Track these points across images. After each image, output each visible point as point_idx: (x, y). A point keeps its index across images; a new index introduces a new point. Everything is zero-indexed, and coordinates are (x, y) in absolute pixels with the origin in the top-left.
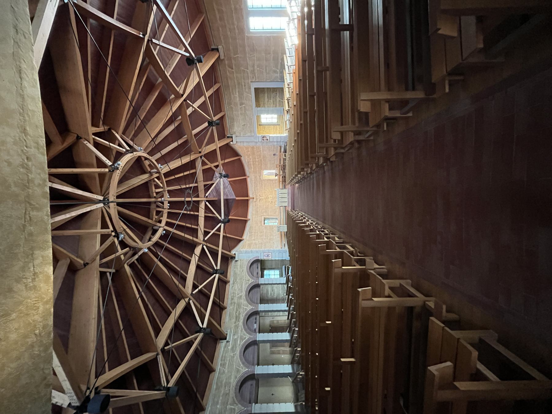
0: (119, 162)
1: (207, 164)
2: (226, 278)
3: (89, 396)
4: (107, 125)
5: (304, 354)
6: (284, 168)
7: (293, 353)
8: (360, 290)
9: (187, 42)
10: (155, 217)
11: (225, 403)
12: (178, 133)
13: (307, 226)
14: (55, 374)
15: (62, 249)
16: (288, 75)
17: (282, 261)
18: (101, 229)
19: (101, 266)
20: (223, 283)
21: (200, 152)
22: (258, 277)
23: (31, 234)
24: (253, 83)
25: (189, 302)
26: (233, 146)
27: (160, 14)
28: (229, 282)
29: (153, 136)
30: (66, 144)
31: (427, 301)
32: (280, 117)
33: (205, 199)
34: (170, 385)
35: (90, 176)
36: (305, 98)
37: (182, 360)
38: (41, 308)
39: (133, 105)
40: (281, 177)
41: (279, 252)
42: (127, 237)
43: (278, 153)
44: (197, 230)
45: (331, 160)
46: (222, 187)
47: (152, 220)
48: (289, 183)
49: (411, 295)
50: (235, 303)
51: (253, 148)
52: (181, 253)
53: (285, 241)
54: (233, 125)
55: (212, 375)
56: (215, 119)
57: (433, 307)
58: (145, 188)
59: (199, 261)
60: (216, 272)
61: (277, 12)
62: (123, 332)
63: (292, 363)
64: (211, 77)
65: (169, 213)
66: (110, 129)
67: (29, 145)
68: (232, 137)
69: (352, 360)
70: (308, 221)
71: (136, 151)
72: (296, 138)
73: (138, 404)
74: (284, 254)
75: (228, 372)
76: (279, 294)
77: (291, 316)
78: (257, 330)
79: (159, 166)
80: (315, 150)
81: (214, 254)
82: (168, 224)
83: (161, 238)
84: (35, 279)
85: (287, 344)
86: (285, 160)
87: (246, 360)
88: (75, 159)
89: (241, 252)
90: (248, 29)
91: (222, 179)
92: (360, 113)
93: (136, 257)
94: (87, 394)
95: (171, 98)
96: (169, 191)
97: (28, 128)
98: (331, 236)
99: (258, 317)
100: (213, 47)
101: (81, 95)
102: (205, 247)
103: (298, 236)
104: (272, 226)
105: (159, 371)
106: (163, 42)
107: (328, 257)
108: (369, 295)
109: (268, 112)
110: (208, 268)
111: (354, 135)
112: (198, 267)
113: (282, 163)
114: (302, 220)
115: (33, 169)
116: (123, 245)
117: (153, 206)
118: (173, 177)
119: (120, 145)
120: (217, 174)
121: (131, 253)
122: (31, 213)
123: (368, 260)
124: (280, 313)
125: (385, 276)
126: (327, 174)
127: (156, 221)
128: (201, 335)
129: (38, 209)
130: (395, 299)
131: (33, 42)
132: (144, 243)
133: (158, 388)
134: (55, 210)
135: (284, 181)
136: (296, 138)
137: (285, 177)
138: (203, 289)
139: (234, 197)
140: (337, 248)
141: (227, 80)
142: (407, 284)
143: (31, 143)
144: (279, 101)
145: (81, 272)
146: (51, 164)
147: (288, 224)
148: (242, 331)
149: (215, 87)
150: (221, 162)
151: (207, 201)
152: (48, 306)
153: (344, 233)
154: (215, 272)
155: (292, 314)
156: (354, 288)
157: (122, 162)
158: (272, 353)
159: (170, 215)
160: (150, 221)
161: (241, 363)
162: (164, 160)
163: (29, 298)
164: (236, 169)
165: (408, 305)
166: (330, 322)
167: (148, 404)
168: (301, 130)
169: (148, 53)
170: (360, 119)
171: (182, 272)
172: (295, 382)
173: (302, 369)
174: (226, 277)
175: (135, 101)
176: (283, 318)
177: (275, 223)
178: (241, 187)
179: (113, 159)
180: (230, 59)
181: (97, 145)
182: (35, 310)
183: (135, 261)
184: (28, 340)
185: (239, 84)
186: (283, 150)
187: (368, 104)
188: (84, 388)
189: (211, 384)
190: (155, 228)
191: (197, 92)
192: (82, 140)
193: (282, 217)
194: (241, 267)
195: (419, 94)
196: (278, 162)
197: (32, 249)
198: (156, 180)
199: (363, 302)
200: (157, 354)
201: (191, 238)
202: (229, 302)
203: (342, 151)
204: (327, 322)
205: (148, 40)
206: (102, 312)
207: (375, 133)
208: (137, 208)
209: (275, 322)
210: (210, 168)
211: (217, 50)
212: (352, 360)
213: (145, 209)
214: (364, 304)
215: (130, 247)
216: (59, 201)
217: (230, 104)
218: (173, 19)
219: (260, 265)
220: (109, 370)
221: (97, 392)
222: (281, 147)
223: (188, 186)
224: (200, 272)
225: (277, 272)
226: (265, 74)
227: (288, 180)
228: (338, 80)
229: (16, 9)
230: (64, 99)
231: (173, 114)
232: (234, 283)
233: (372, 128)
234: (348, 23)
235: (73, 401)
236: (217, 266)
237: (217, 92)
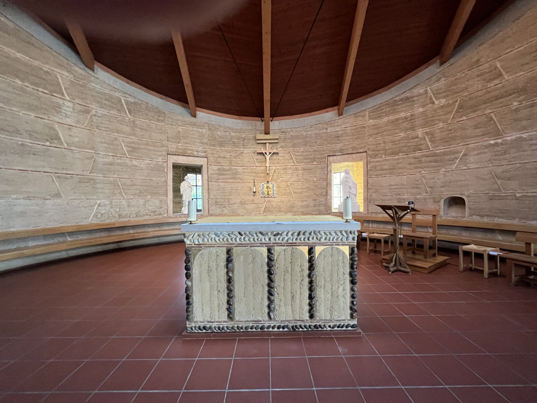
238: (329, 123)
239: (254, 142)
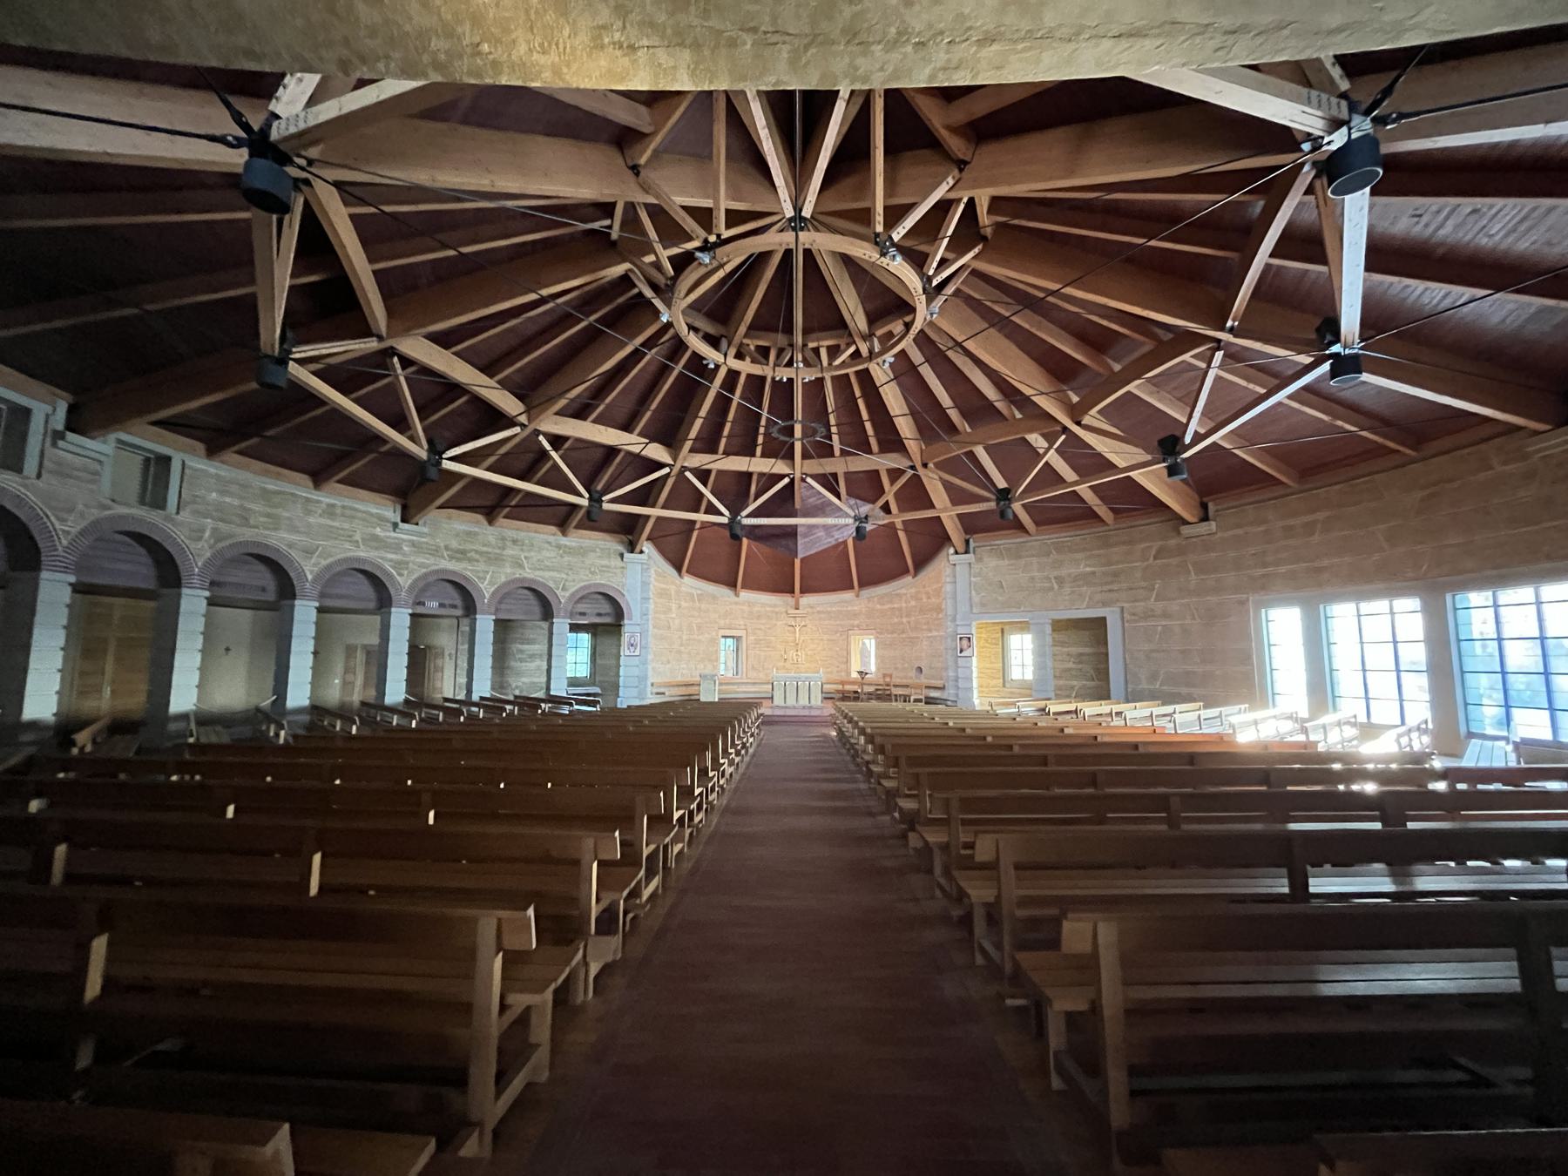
0: (899, 258)
1: (892, 482)
2: (577, 527)
3: (291, 163)
4: (995, 232)
5: (340, 744)
6: (883, 696)
7: (344, 713)
8: (531, 912)
9: (1223, 438)
10: (752, 344)
11: (221, 513)
12: (978, 410)
13: (715, 760)
14: (361, 84)
15: (682, 109)
16: (1146, 713)
17: (616, 687)
18: (728, 211)
19: (631, 207)
20: (562, 517)
22: (571, 615)
23: (733, 43)
24: (1118, 616)
26: (943, 554)
27: (1290, 372)
28: (564, 534)
29: (969, 345)
30: (944, 135)
31: (481, 1134)
32: (1026, 689)
33: (798, 475)
34: (293, 368)
35: (866, 187)
36: (1083, 760)
37: (356, 401)
38: (542, 59)
39: (1050, 299)
40: (855, 688)
41: (643, 678)
42: (702, 271)
43: (924, 681)
44: (714, 451)
45: (911, 835)
46: (830, 521)
47: (746, 336)
48: (839, 709)
49: (502, 1079)
51: (939, 609)
52: (654, 406)
53: (671, 695)
54: (1001, 556)
55: (305, 479)
57: (463, 1153)
58: (829, 320)
59: (629, 453)
60: (596, 499)
61: (1321, 688)
62: (452, 253)
63: (316, 710)
64: (1131, 500)
66: (984, 239)
67: (955, 48)
68: (967, 552)
69: (314, 889)
70: (731, 763)
71: (929, 301)
72: (968, 731)
73: (252, 281)
74: (634, 692)
75: (309, 525)
76: (519, 674)
77: (452, 709)
78: (420, 610)
79: (889, 358)
80: (932, 785)
81: (644, 496)
82: (733, 375)
83: (697, 358)
84: (621, 47)
85: (371, 694)
86: (906, 699)
87: (339, 574)
88: (909, 153)
89: (645, 570)
90: (1269, 604)
91: (851, 521)
92: (1057, 922)
93: (648, 293)
94: (297, 160)
95: (1070, 393)
96: (820, 381)
97: (995, 47)
98: (688, 831)
99: (459, 612)
100: (1211, 507)
101: (1070, 173)
102: (667, 470)
103: (686, 734)
104: (717, 660)
105: (343, 339)
106: (1218, 379)
107: (626, 820)
108: (512, 942)
109: (1039, 653)
110: (606, 478)
111: (987, 905)
112: (612, 451)
113: (899, 691)
114: (734, 745)
115: (895, 56)
116: (683, 262)
117: (781, 339)
118: (858, 393)
119: (943, 262)
120: (865, 509)
121: (661, 281)
122: (786, 48)
123: (615, 941)
124: (468, 677)
125: (562, 997)
126: (868, 821)
127: (741, 344)
128: (422, 453)
129: (793, 62)
130: (493, 1025)
131: (1208, 66)
132: (683, 312)
133: (289, 334)
134: (779, 103)
135: (845, 697)
136: (968, 731)
137: (856, 699)
139: (800, 555)
140: (652, 847)
141: (1124, 543)
142: (537, 1067)
143: (960, 51)
144: (1073, 688)
146: (893, 96)
147: (723, 703)
148: (422, 565)
149: (1102, 511)
151: (792, 480)
152: (547, 75)
153: (693, 872)
154: (596, 496)
155: (459, 712)
156: (536, 897)
157: (899, 266)
158: (350, 651)
159: (756, 382)
160: (743, 329)
161: (330, 560)
162: (904, 370)
163: (574, 33)
164: (877, 562)
165: (473, 1070)
166: (431, 822)
167: (247, 311)
168: (991, 746)
169: (1194, 340)
170: (1034, 923)
171: (601, 408)
172: (256, 716)
173: (295, 737)
174: (578, 527)
175: (1060, 303)
176: (447, 685)
177: (724, 669)
178: (829, 575)
179: (908, 243)
180: (1181, 551)
181: (944, 207)
182: (541, 45)
183: (636, 291)
184: (467, 27)
185: (1116, 575)
186: (934, 694)
187: (1084, 947)
188: (313, 152)
189: (278, 476)
190: (724, 343)
192: (956, 172)
193: (743, 688)
194: (604, 569)
195: (1119, 1114)
196: (898, 681)
197: (696, 46)
198: (852, 349)
199: (494, 922)
200: (380, 338)
201: (693, 434)
203: (938, 870)
204: (432, 814)
205: (1219, 341)
206: (510, 204)
207: (993, 971)
208: (775, 299)
209: (439, 662)
210: (883, 492)
211: (1205, 518)
212: (314, 889)
213: (775, 318)
214: (487, 923)
215: (675, 279)
216: (799, 114)
217: (1059, 548)
218: (1280, 404)
219: (607, 624)
220: (352, 217)
221: (298, 184)
222: (942, 688)
223: (834, 429)
224: (598, 455)
225: (583, 671)
226: (1147, 647)
227: (846, 706)
228: (1147, 856)
229: (1286, 32)
230: (1060, 133)
231: (1028, 398)
232: (559, 547)
233: (1013, 959)
234: (1312, 890)
235: (283, 125)
236: (613, 501)
237: (1091, 515)
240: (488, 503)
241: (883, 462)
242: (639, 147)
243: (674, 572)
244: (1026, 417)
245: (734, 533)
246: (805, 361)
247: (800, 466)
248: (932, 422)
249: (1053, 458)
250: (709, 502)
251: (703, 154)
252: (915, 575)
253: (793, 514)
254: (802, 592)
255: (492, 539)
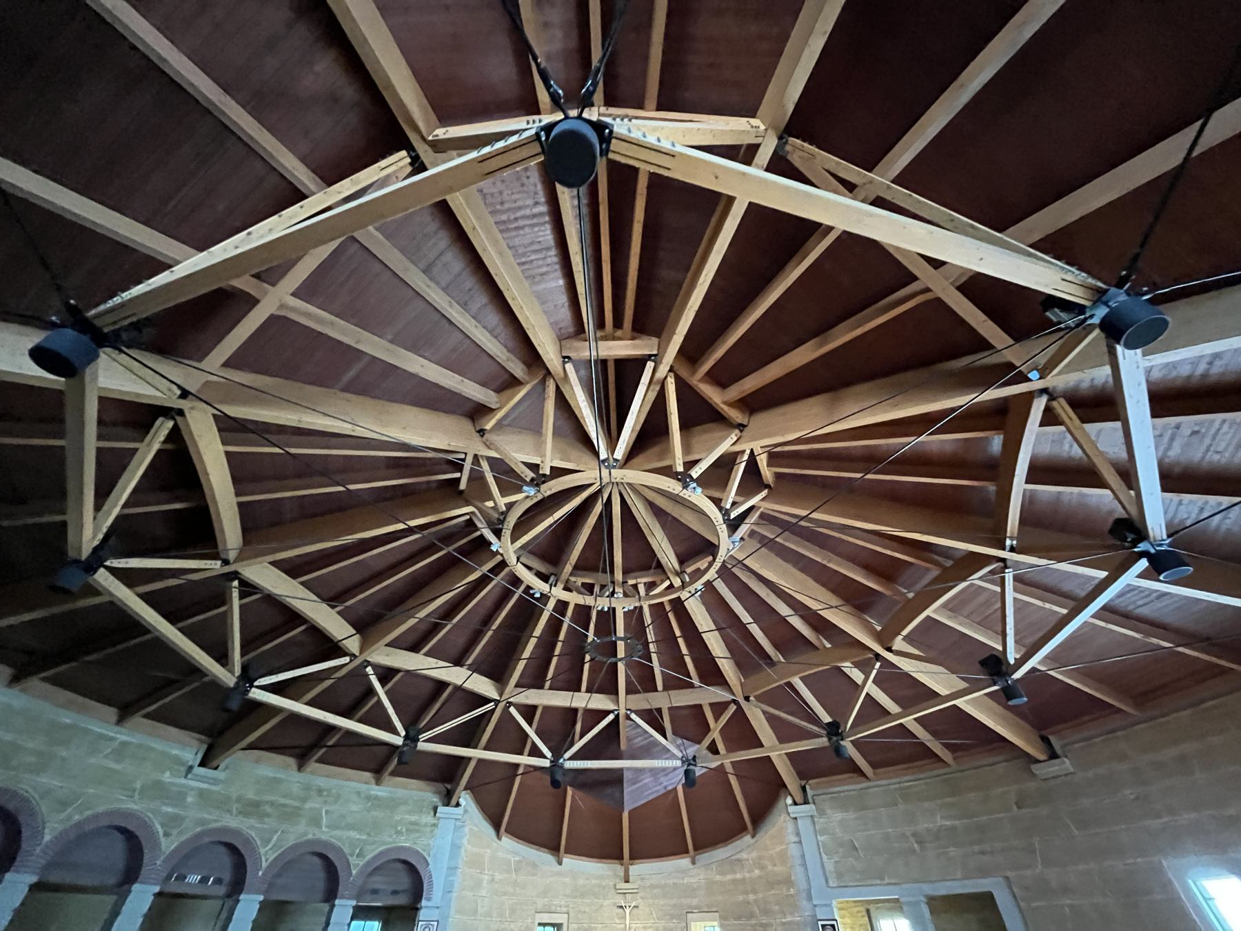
0: (699, 490)
1: (717, 719)
10: (579, 581)
12: (789, 641)
20: (379, 761)
21: (747, 699)
25: (345, 654)
26: (781, 804)
33: (622, 712)
35: (668, 451)
47: (571, 575)
50: (304, 800)
54: (844, 807)
56: (847, 744)
65: (588, 609)
68: (806, 802)
78: (174, 887)
81: (467, 735)
88: (699, 428)
91: (679, 763)
102: (491, 706)
112: (441, 685)
118: (678, 633)
120: (692, 750)
127: (567, 581)
138: (375, 699)
139: (628, 807)
145: (467, 425)
148: (202, 822)
150: (727, 762)
151: (617, 716)
159: (583, 613)
160: (568, 568)
174: (393, 774)
183: (478, 533)
191: (912, 693)
198: (667, 583)
202: (321, 782)
205: (1003, 560)
210: (707, 729)
213: (595, 560)
223: (652, 647)
232: (368, 798)
237: (929, 754)
238: (684, 872)
239: (613, 891)
240: (305, 743)
241: (707, 695)
242: (487, 417)
243: (491, 831)
244: (835, 645)
245: (556, 778)
246: (626, 595)
247: (624, 703)
248: (749, 657)
249: (871, 688)
250: (533, 743)
251: (536, 429)
252: (753, 836)
253: (618, 756)
254: (696, 848)
255: (295, 789)
